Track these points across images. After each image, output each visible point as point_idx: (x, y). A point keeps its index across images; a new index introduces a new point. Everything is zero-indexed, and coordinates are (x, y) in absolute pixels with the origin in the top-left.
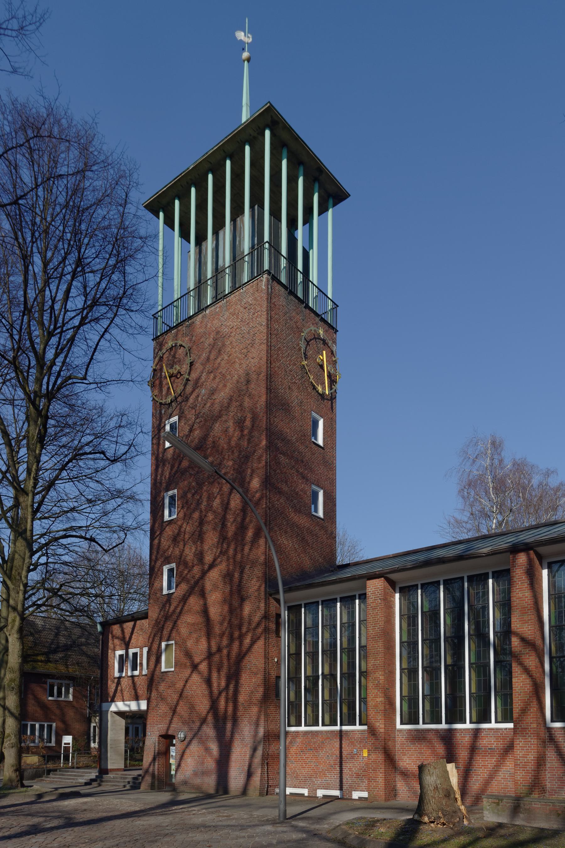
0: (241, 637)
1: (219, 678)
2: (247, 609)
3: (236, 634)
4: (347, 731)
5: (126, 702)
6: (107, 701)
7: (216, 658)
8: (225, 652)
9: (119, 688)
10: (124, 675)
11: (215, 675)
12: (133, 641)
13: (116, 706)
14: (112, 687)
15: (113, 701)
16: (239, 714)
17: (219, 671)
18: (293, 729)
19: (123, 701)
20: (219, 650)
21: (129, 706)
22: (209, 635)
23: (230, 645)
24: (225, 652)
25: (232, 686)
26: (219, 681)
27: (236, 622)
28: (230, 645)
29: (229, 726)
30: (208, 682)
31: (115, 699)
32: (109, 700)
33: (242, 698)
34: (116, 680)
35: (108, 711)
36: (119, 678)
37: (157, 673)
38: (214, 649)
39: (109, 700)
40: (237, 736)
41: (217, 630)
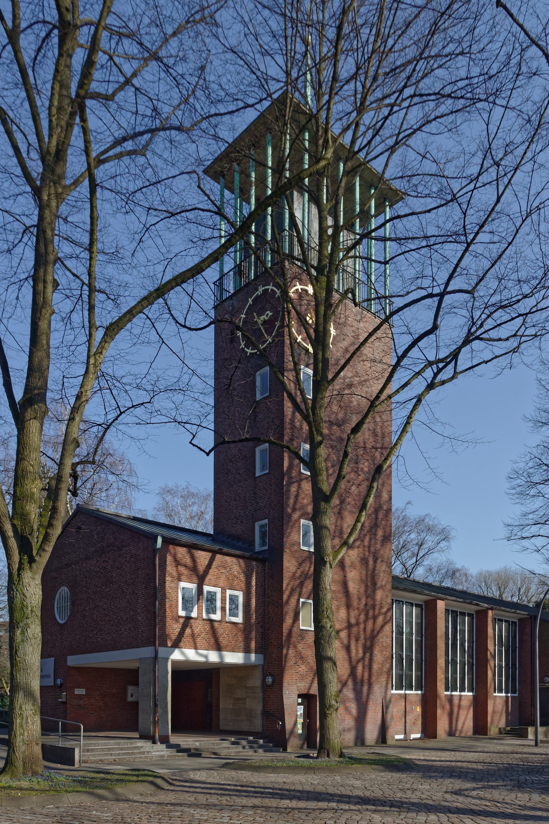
0: (375, 618)
1: (357, 646)
2: (379, 595)
3: (371, 613)
4: (409, 694)
5: (200, 651)
6: (166, 646)
7: (355, 630)
8: (362, 626)
9: (188, 631)
10: (194, 614)
11: (353, 643)
12: (209, 577)
13: (183, 654)
14: (174, 629)
15: (176, 645)
16: (374, 679)
17: (357, 640)
18: (497, 694)
19: (196, 648)
20: (358, 624)
21: (206, 657)
22: (348, 606)
23: (366, 621)
24: (362, 626)
25: (368, 655)
26: (357, 651)
27: (370, 602)
28: (366, 621)
29: (365, 689)
30: (348, 649)
31: (181, 644)
32: (169, 644)
33: (375, 667)
34: (182, 621)
35: (168, 658)
36: (188, 618)
37: (295, 629)
38: (353, 621)
39: (169, 644)
40: (372, 697)
41: (355, 603)
